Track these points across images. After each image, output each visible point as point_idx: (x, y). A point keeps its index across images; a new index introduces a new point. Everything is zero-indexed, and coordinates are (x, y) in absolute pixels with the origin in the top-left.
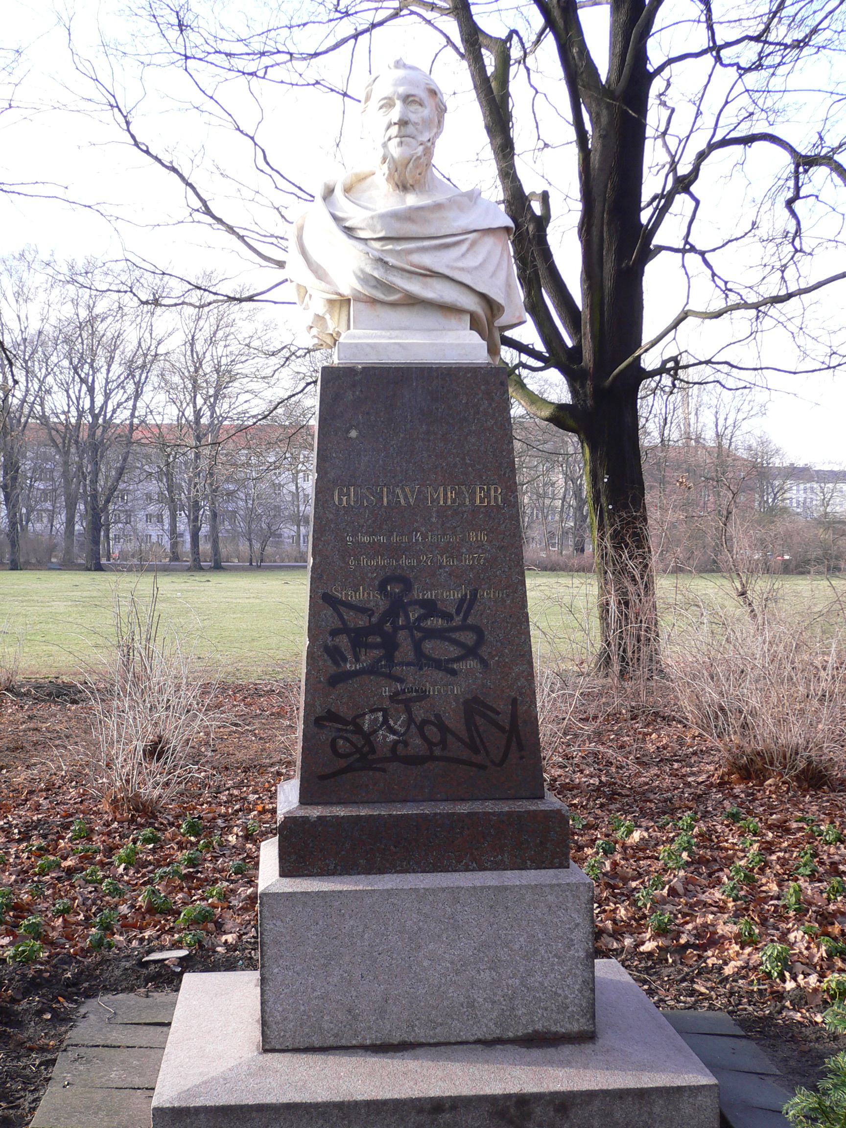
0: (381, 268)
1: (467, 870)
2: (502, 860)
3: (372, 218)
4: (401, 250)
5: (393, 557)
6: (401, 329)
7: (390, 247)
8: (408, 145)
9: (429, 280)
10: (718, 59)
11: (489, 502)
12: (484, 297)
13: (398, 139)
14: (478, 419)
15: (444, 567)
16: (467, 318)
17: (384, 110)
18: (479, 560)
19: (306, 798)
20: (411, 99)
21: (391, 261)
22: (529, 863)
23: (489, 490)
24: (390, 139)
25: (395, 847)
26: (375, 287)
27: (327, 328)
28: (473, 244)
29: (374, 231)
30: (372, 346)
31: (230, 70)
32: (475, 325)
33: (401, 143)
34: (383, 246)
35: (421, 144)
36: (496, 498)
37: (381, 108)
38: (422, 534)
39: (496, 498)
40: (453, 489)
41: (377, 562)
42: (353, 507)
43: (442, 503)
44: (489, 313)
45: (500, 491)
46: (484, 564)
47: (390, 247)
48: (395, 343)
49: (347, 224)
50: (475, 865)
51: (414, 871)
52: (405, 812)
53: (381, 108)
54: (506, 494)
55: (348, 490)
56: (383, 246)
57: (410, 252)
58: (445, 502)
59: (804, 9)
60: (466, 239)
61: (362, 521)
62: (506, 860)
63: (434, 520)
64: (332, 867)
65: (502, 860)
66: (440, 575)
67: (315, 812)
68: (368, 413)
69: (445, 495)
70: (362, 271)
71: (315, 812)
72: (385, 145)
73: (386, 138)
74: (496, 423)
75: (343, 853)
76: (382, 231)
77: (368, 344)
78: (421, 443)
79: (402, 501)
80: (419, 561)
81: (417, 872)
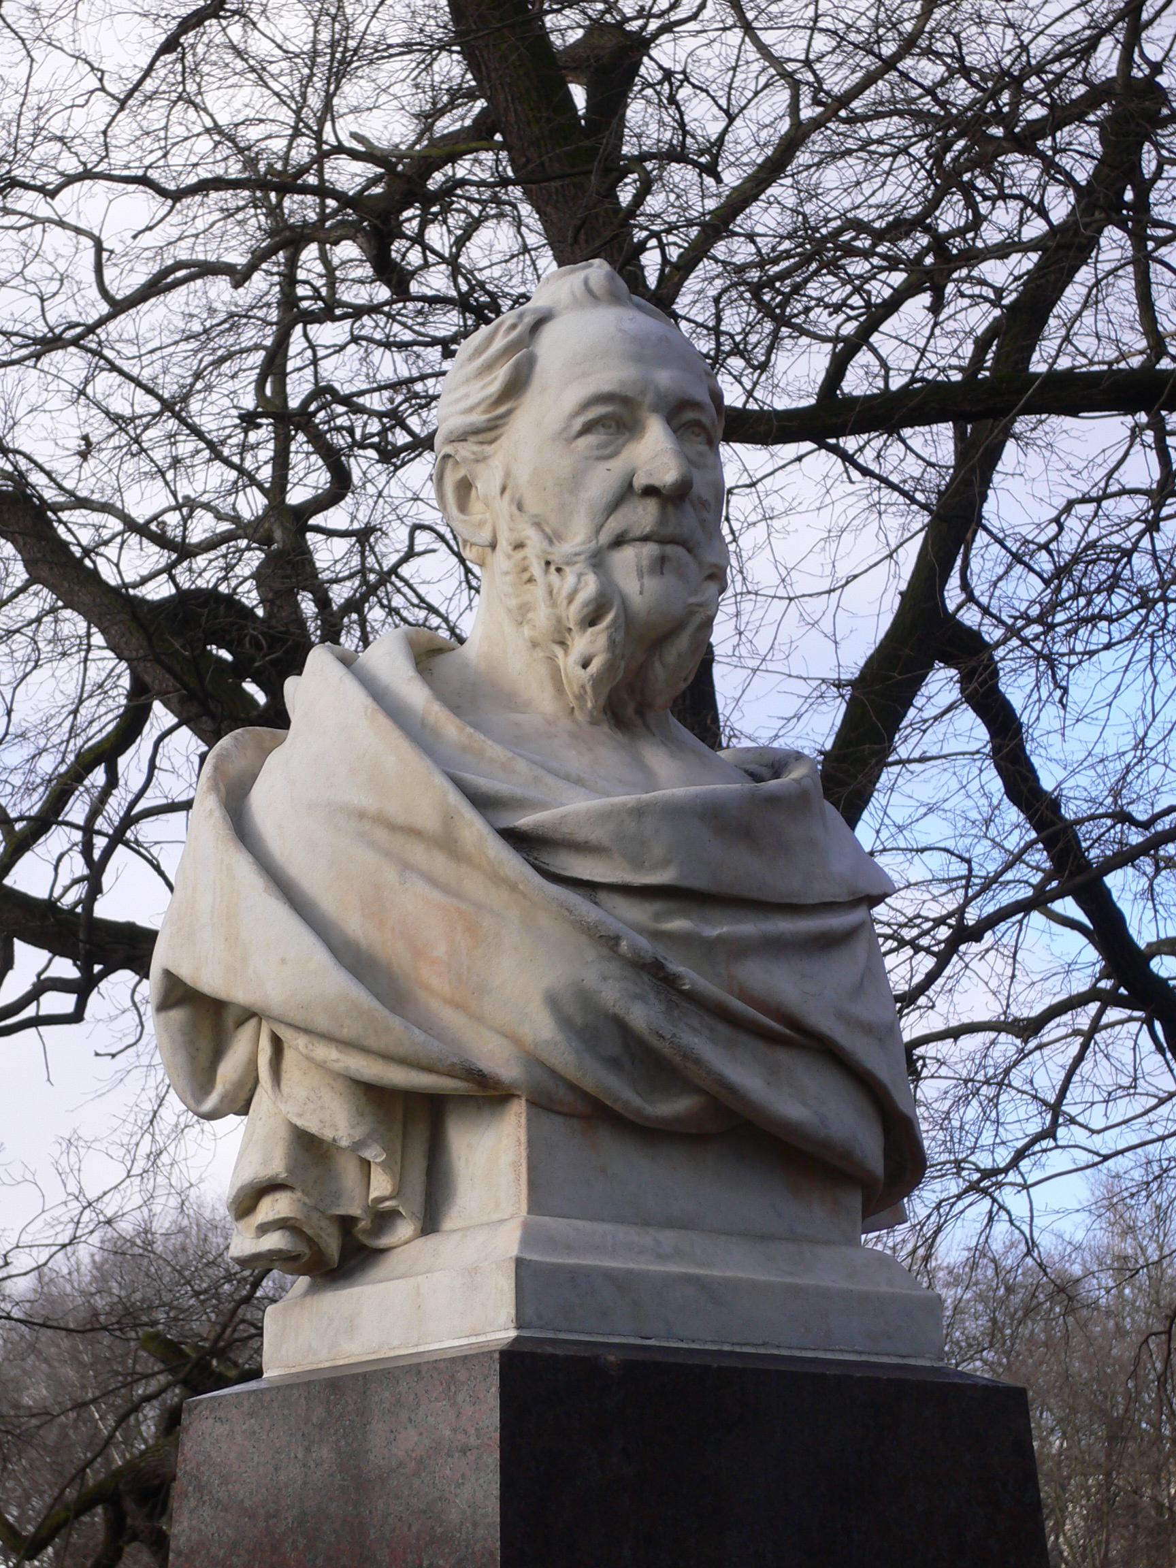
0: (652, 997)
3: (639, 812)
4: (720, 940)
6: (670, 1223)
7: (678, 924)
8: (681, 574)
9: (782, 1056)
10: (8, 340)
13: (649, 550)
20: (689, 415)
21: (691, 976)
26: (613, 1063)
27: (337, 1195)
29: (637, 864)
30: (620, 1282)
33: (660, 564)
34: (657, 917)
37: (587, 429)
47: (678, 924)
48: (689, 1279)
49: (525, 821)
53: (587, 429)
57: (739, 949)
59: (157, 218)
70: (586, 999)
72: (598, 561)
73: (605, 537)
76: (665, 863)
77: (610, 1277)
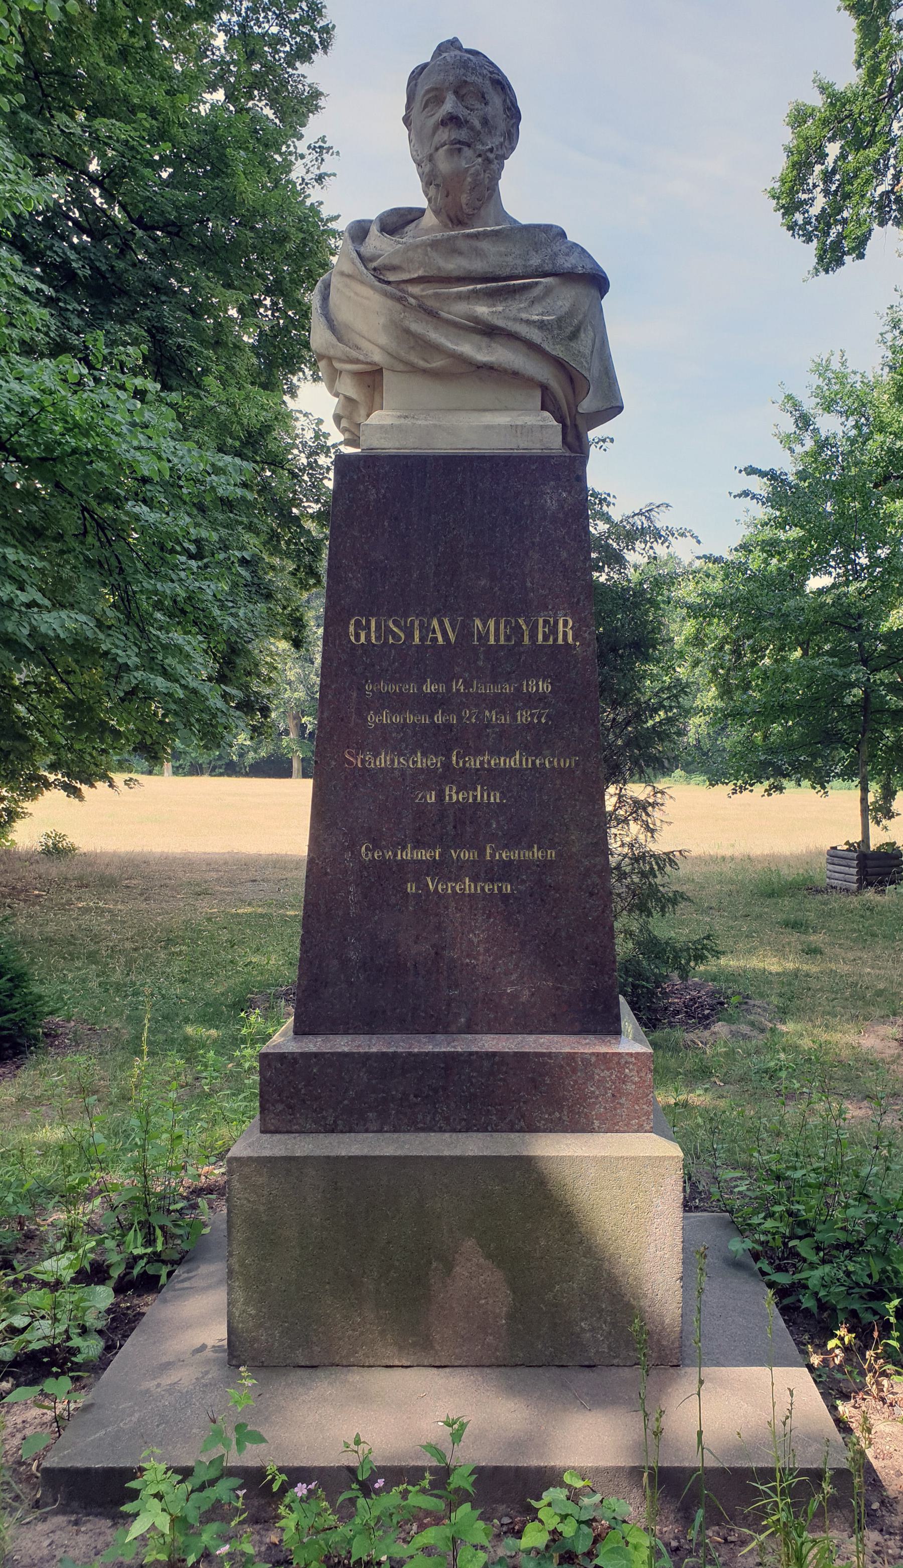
1: (512, 1130)
2: (560, 1118)
5: (425, 712)
11: (556, 640)
12: (559, 364)
14: (545, 527)
15: (493, 726)
16: (538, 394)
17: (431, 106)
18: (539, 718)
19: (300, 1030)
22: (597, 1123)
23: (556, 623)
24: (437, 149)
25: (416, 1096)
28: (548, 291)
31: (604, 441)
32: (548, 403)
34: (423, 290)
35: (480, 156)
36: (565, 634)
38: (464, 682)
39: (565, 634)
40: (507, 623)
41: (405, 719)
42: (374, 645)
43: (492, 641)
44: (569, 391)
45: (570, 623)
46: (546, 723)
50: (522, 1123)
51: (441, 1130)
52: (429, 1048)
54: (580, 629)
55: (368, 622)
56: (423, 290)
58: (497, 639)
60: (537, 283)
61: (385, 664)
62: (565, 1118)
63: (481, 663)
64: (330, 1120)
65: (560, 1118)
66: (488, 735)
67: (313, 1045)
68: (396, 519)
69: (497, 630)
71: (313, 1045)
74: (568, 533)
75: (346, 1102)
78: (466, 560)
79: (440, 639)
80: (460, 718)
81: (445, 1131)
